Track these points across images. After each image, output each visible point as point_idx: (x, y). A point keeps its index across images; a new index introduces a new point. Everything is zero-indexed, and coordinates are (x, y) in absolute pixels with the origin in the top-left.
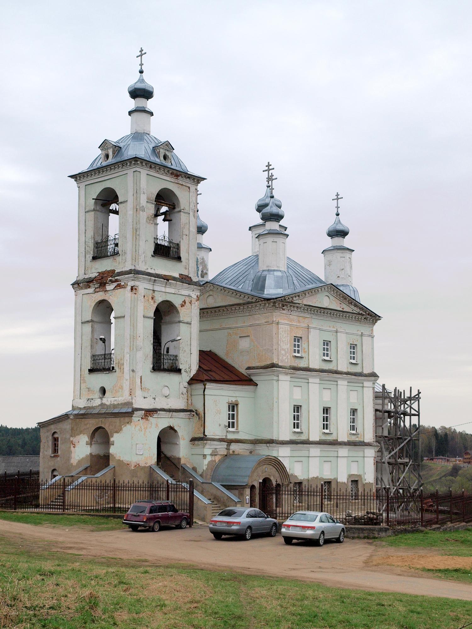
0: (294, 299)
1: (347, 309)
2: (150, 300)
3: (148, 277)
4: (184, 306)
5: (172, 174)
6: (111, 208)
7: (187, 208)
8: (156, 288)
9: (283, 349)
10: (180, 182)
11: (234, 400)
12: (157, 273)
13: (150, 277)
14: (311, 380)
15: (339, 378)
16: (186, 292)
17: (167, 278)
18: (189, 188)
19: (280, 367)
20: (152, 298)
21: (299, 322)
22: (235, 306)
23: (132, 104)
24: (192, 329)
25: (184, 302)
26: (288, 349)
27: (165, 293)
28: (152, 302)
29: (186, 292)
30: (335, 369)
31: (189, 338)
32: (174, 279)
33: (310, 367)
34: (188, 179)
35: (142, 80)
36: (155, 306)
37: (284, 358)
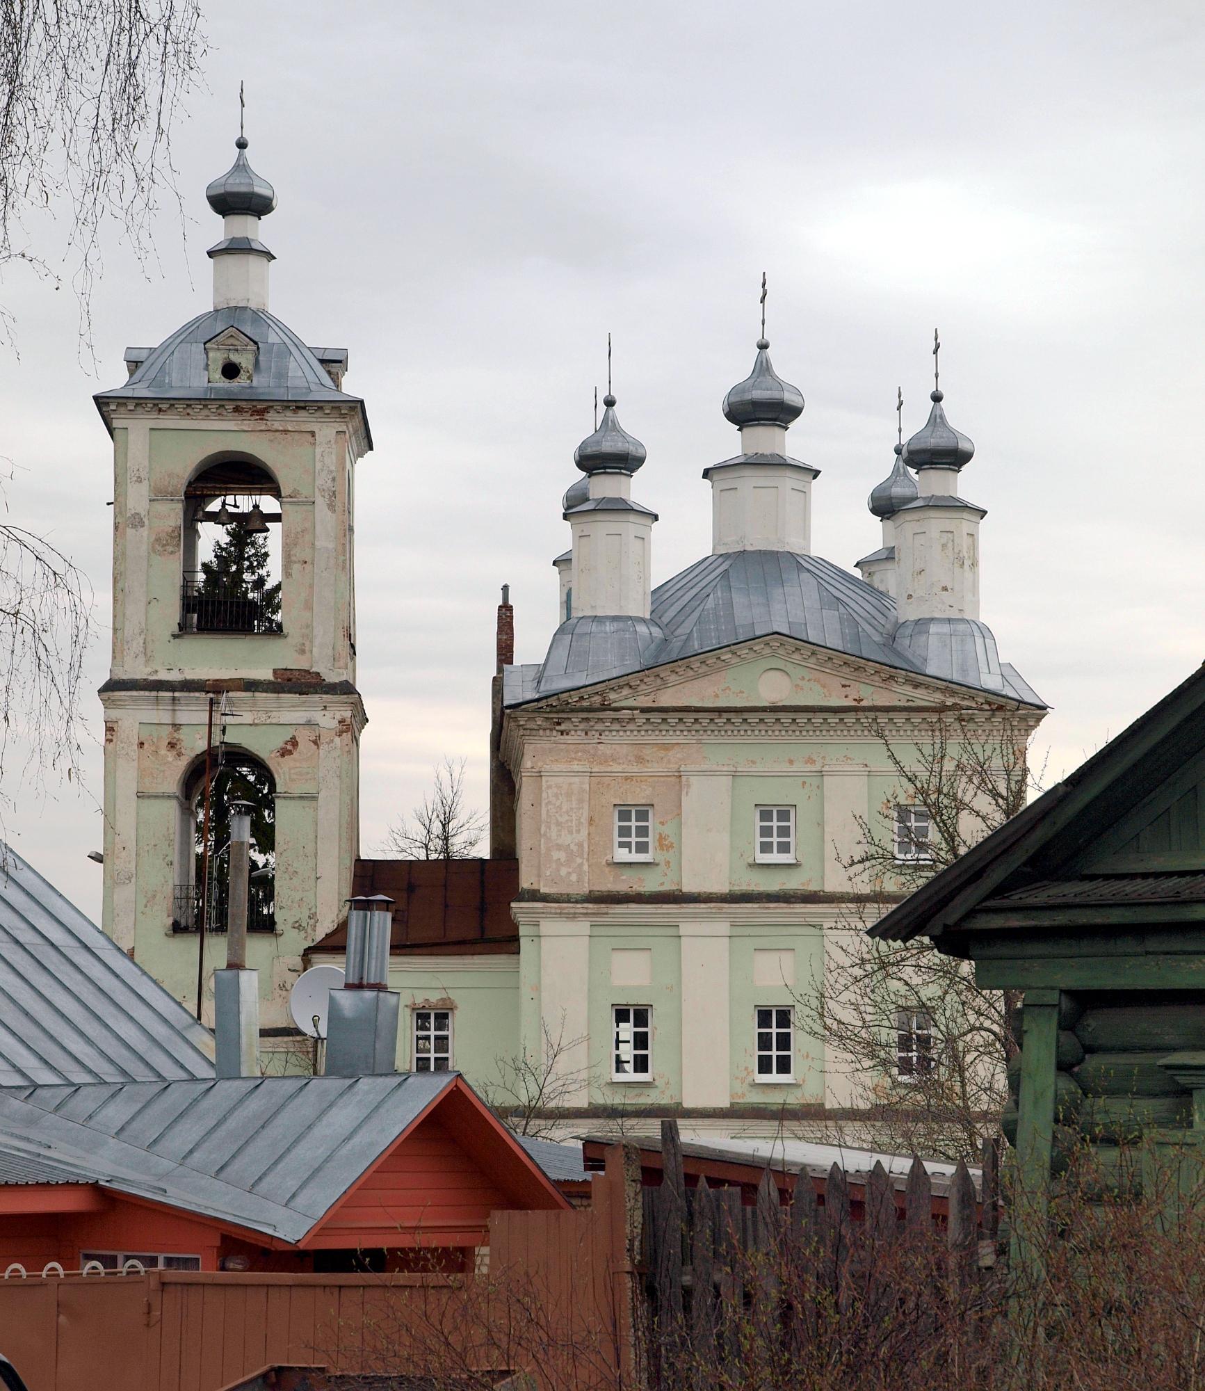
0: (613, 696)
2: (163, 752)
3: (147, 693)
4: (290, 753)
5: (237, 410)
6: (208, 509)
7: (305, 491)
9: (559, 847)
10: (277, 426)
11: (434, 997)
12: (189, 677)
13: (154, 694)
14: (685, 929)
16: (299, 716)
18: (313, 434)
19: (545, 898)
20: (172, 745)
21: (640, 760)
22: (826, 715)
23: (217, 229)
24: (321, 813)
25: (294, 742)
26: (580, 845)
28: (170, 756)
29: (299, 716)
30: (813, 887)
31: (312, 837)
32: (251, 686)
33: (685, 890)
34: (302, 413)
35: (241, 167)
36: (182, 764)
37: (563, 872)
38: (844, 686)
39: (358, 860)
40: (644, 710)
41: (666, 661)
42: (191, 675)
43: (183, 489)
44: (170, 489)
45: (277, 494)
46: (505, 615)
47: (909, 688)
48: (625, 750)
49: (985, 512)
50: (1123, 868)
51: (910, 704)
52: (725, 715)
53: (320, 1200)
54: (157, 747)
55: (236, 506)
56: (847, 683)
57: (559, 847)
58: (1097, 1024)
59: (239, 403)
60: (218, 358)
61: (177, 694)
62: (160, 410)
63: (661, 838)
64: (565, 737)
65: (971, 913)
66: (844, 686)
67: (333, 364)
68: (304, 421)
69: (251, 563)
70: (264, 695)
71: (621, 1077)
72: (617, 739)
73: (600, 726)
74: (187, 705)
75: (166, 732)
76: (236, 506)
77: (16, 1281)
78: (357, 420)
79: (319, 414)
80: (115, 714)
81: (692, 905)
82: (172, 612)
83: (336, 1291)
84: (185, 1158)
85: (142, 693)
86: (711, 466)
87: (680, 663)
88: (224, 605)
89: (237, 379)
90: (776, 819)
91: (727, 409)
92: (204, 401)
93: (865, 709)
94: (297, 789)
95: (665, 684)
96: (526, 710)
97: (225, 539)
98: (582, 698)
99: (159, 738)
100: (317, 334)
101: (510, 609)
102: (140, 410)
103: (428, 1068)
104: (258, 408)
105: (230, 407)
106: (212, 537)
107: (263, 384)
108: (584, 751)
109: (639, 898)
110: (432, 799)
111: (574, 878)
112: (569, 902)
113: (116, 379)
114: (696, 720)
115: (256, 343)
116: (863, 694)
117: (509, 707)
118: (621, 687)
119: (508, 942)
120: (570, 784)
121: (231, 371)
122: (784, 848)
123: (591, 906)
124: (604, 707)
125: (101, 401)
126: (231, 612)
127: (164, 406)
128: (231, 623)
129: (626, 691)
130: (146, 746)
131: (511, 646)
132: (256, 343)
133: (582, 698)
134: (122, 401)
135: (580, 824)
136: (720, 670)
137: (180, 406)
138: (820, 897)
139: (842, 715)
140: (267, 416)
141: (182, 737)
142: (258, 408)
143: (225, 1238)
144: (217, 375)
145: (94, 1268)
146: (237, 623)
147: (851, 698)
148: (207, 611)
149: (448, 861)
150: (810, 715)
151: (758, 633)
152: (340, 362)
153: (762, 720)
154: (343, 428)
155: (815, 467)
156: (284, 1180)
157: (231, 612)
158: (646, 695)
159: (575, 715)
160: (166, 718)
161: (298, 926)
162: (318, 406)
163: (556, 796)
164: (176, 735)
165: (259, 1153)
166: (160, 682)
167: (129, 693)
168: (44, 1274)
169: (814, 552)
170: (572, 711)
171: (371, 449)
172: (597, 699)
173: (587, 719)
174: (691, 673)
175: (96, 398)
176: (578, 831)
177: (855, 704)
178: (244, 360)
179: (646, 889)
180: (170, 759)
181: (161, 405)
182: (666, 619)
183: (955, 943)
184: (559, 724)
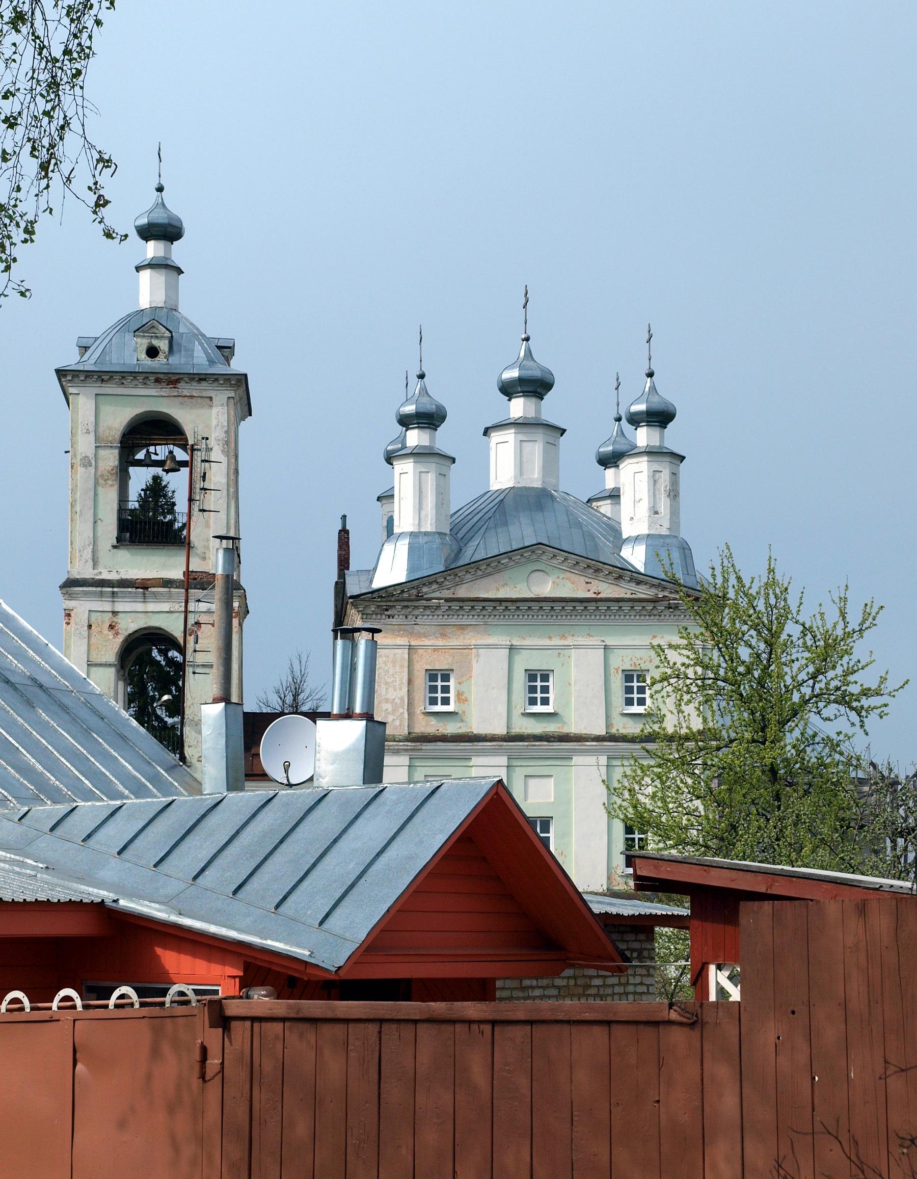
0: (425, 589)
1: (608, 590)
2: (106, 631)
3: (94, 589)
5: (157, 381)
8: (120, 607)
9: (387, 701)
10: (186, 393)
12: (124, 577)
13: (99, 589)
15: (575, 751)
17: (144, 585)
18: (211, 398)
20: (111, 627)
21: (443, 635)
26: (402, 699)
27: (136, 615)
28: (110, 635)
32: (167, 583)
34: (204, 384)
36: (120, 639)
38: (587, 583)
40: (447, 600)
41: (453, 571)
44: (110, 439)
45: (184, 447)
46: (344, 536)
47: (634, 584)
48: (433, 629)
49: (684, 458)
51: (634, 596)
52: (504, 604)
53: (357, 922)
54: (102, 628)
55: (156, 454)
56: (590, 580)
57: (387, 701)
59: (159, 376)
60: (143, 343)
61: (115, 590)
62: (103, 380)
63: (459, 694)
64: (391, 619)
66: (587, 583)
67: (226, 350)
68: (205, 389)
69: (163, 510)
70: (177, 590)
72: (428, 622)
73: (416, 612)
74: (123, 597)
75: (108, 618)
76: (156, 454)
77: (17, 1016)
78: (242, 390)
79: (216, 384)
80: (71, 604)
81: (481, 744)
83: (487, 1028)
84: (195, 878)
85: (90, 589)
86: (490, 425)
87: (472, 565)
88: (148, 525)
89: (157, 359)
90: (537, 681)
91: (501, 384)
92: (134, 374)
93: (601, 600)
95: (461, 582)
96: (364, 600)
98: (403, 591)
99: (103, 622)
101: (347, 532)
102: (89, 380)
103: (639, 676)
104: (171, 380)
105: (152, 378)
106: (140, 478)
107: (178, 362)
108: (405, 631)
109: (444, 739)
110: (286, 679)
111: (397, 723)
112: (395, 741)
113: (71, 359)
114: (484, 607)
115: (171, 332)
116: (600, 589)
117: (351, 597)
118: (430, 583)
120: (395, 654)
122: (545, 701)
123: (410, 744)
124: (419, 597)
125: (61, 373)
126: (154, 530)
127: (105, 378)
128: (153, 537)
129: (434, 586)
130: (93, 627)
131: (348, 559)
132: (171, 332)
133: (403, 591)
134: (75, 374)
135: (402, 683)
136: (500, 571)
137: (117, 377)
138: (571, 737)
139: (585, 604)
140: (178, 385)
141: (119, 621)
142: (171, 380)
143: (247, 967)
144: (143, 356)
145: (122, 996)
146: (157, 537)
147: (592, 591)
148: (136, 528)
150: (563, 604)
151: (526, 545)
152: (229, 348)
153: (530, 608)
154: (233, 395)
155: (562, 427)
156: (311, 900)
157: (154, 530)
158: (448, 589)
159: (398, 603)
160: (107, 607)
163: (385, 663)
164: (115, 619)
165: (280, 872)
166: (103, 580)
167: (81, 589)
168: (55, 1005)
169: (562, 488)
170: (396, 601)
171: (250, 415)
172: (414, 592)
173: (407, 607)
174: (480, 573)
175: (58, 371)
176: (401, 689)
177: (595, 596)
178: (163, 345)
179: (449, 731)
180: (111, 637)
182: (460, 535)
184: (387, 610)
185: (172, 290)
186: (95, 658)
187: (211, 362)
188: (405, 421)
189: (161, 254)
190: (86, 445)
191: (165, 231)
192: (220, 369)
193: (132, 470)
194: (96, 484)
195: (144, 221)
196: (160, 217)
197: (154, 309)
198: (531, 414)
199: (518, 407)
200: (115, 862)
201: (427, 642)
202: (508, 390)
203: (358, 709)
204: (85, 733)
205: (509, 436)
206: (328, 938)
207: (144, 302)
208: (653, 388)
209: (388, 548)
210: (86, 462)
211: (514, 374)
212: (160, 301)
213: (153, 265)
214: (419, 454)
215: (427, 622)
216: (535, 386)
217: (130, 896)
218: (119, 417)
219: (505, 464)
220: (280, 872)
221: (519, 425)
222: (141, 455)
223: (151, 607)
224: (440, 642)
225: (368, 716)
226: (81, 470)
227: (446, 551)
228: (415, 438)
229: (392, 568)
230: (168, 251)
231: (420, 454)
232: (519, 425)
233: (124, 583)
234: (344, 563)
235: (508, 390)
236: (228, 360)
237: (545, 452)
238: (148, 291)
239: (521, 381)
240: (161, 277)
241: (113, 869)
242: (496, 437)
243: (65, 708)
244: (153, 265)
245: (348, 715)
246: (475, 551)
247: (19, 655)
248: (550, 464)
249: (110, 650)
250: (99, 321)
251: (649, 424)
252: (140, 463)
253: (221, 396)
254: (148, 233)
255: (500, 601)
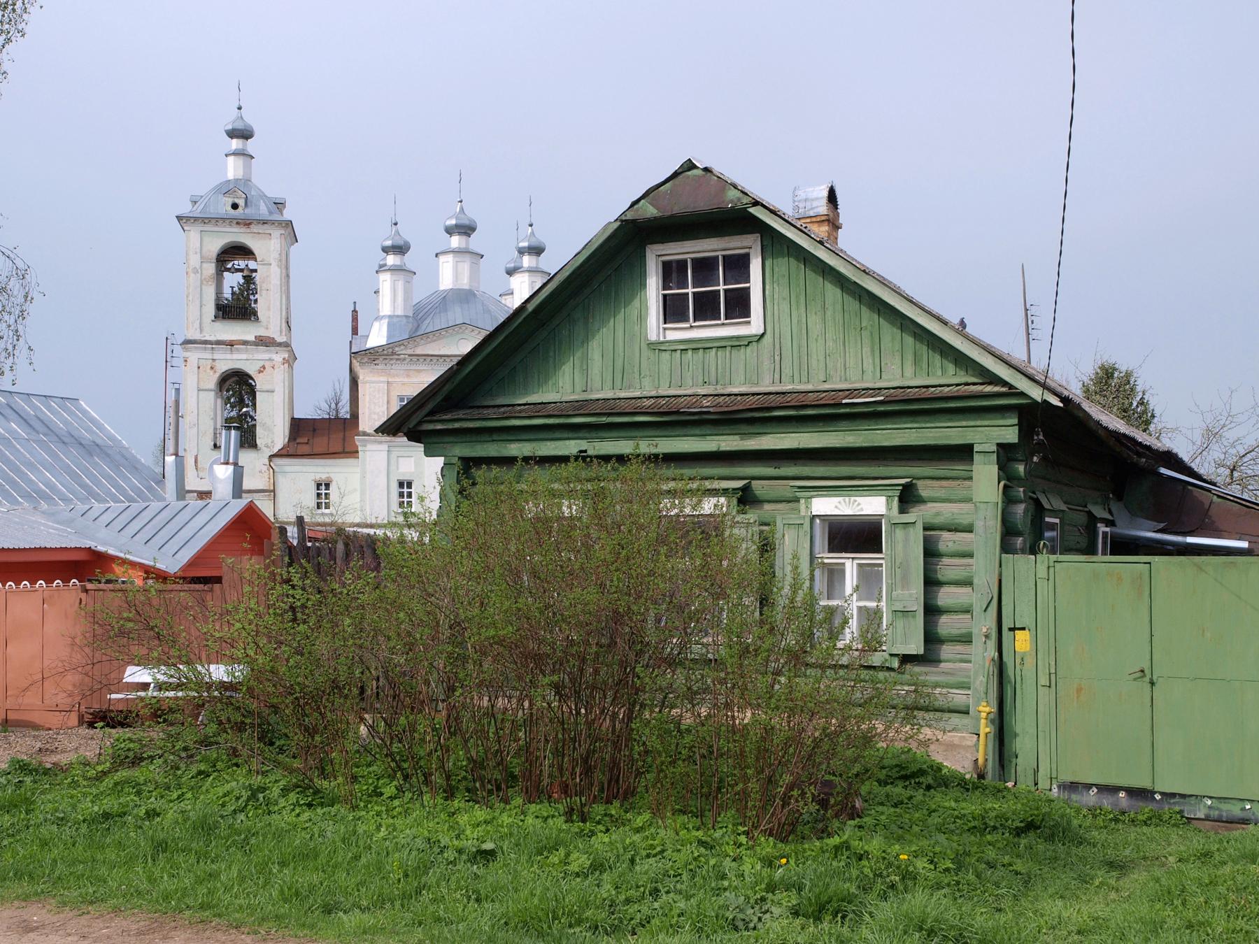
11: (324, 477)
16: (266, 356)
17: (231, 344)
21: (408, 376)
25: (264, 367)
27: (228, 361)
29: (266, 356)
32: (245, 343)
36: (217, 375)
39: (293, 419)
41: (414, 337)
42: (220, 338)
43: (214, 255)
50: (492, 403)
58: (480, 473)
60: (230, 201)
65: (420, 423)
67: (279, 205)
71: (320, 511)
80: (187, 354)
82: (210, 309)
92: (223, 219)
94: (265, 388)
97: (242, 281)
100: (273, 192)
113: (186, 209)
119: (354, 453)
121: (235, 206)
124: (393, 353)
125: (179, 218)
134: (188, 218)
142: (246, 223)
149: (337, 418)
161: (267, 446)
162: (273, 222)
165: (159, 540)
169: (482, 289)
178: (241, 202)
181: (205, 220)
183: (414, 436)
185: (247, 168)
186: (203, 386)
187: (271, 213)
188: (386, 250)
189: (241, 146)
190: (195, 260)
191: (244, 134)
192: (276, 217)
193: (226, 274)
194: (202, 283)
195: (230, 127)
196: (239, 125)
197: (236, 180)
198: (463, 246)
199: (455, 241)
200: (104, 530)
201: (397, 379)
202: (450, 231)
203: (231, 460)
204: (116, 466)
205: (450, 258)
206: (172, 563)
207: (231, 175)
208: (533, 233)
209: (376, 324)
210: (195, 271)
211: (453, 222)
212: (240, 175)
213: (236, 154)
214: (395, 270)
215: (398, 368)
216: (466, 230)
217: (104, 544)
218: (215, 244)
219: (448, 275)
220: (159, 540)
221: (454, 252)
222: (229, 266)
223: (235, 356)
224: (406, 380)
225: (236, 464)
226: (192, 275)
227: (410, 326)
228: (391, 260)
229: (377, 337)
230: (245, 145)
231: (395, 270)
232: (454, 252)
233: (219, 343)
234: (355, 331)
235: (450, 231)
236: (281, 212)
237: (471, 267)
238: (233, 169)
239: (456, 226)
240: (240, 161)
241: (103, 533)
242: (442, 258)
243: (108, 455)
244: (236, 154)
245: (227, 463)
246: (427, 326)
247: (88, 430)
248: (474, 274)
249: (212, 381)
250: (204, 185)
251: (530, 254)
252: (228, 270)
253: (277, 233)
254: (233, 134)
255: (441, 356)
